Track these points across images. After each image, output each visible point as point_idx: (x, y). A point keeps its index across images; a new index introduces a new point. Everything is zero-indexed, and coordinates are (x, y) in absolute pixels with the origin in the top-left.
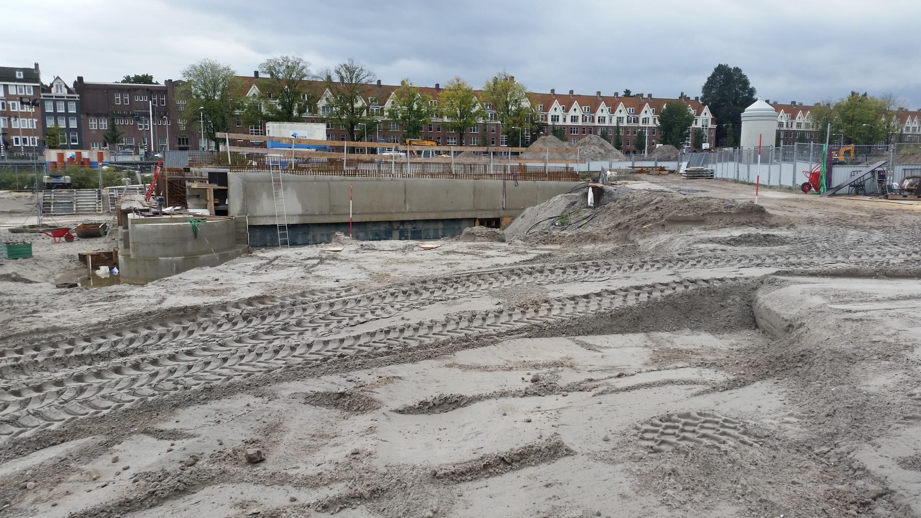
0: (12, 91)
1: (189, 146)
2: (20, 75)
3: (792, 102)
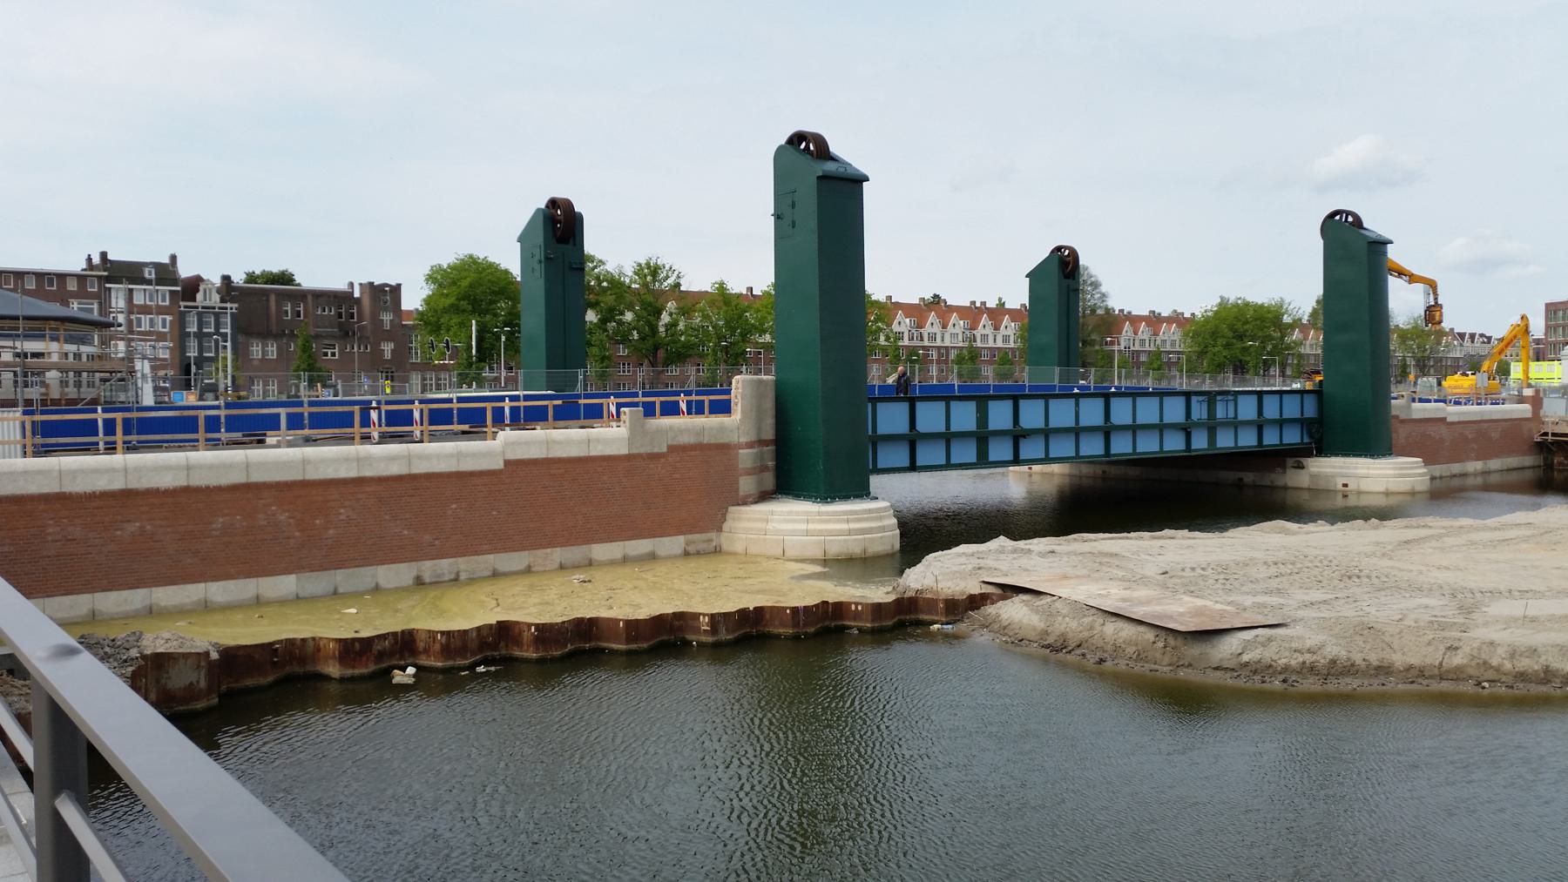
0: (139, 299)
3: (1150, 312)
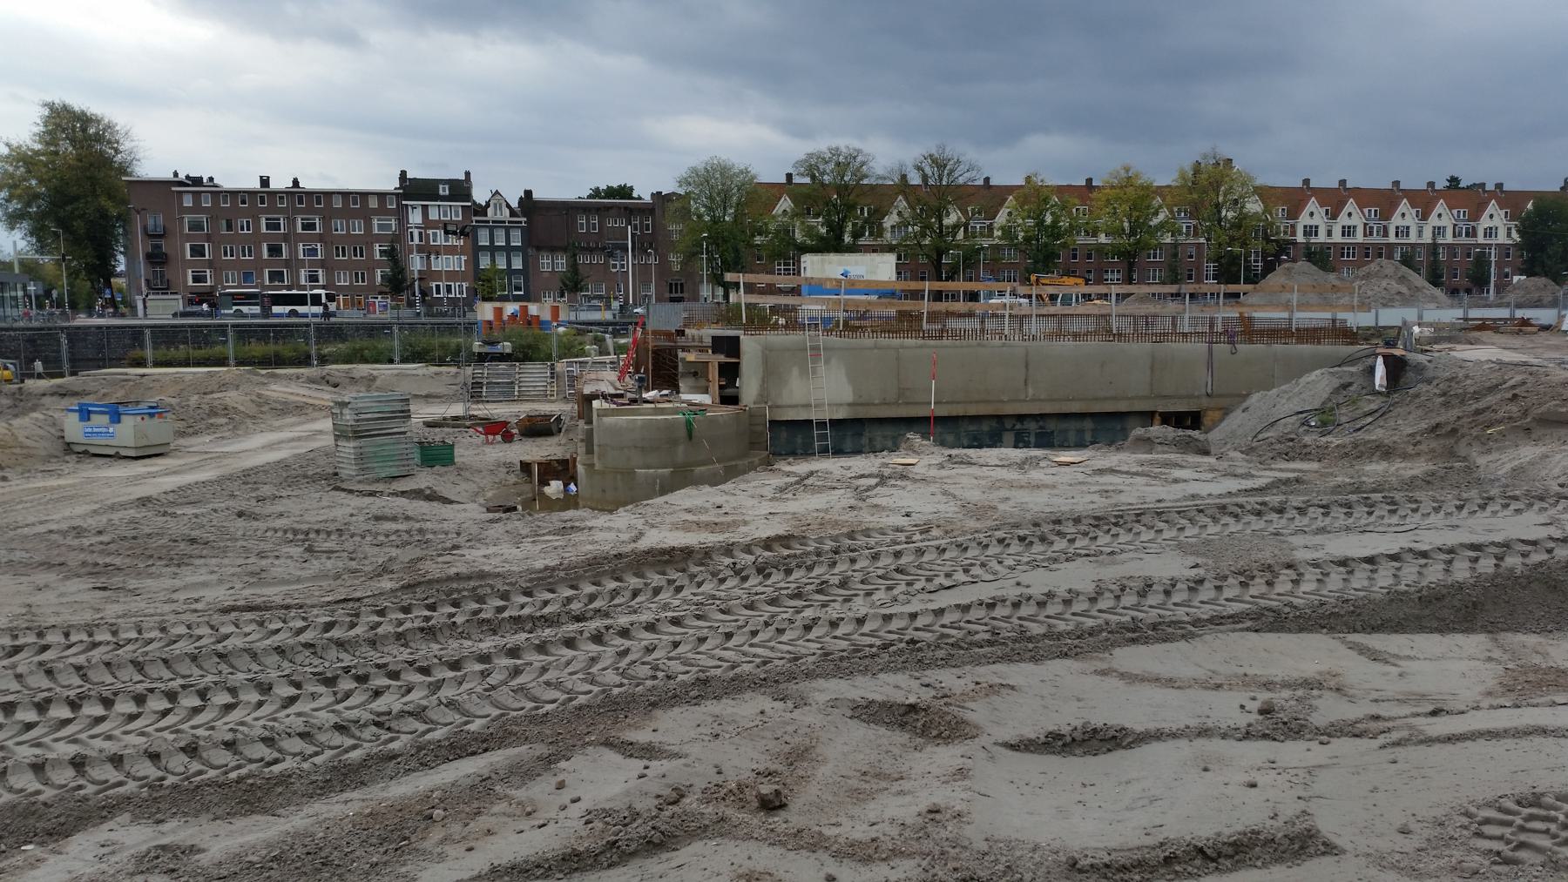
0: (434, 215)
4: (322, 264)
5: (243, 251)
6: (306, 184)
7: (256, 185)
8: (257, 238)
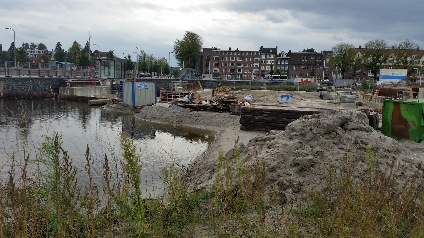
0: (268, 57)
1: (329, 77)
2: (271, 51)
4: (242, 68)
5: (226, 65)
6: (240, 49)
7: (228, 50)
8: (229, 62)
